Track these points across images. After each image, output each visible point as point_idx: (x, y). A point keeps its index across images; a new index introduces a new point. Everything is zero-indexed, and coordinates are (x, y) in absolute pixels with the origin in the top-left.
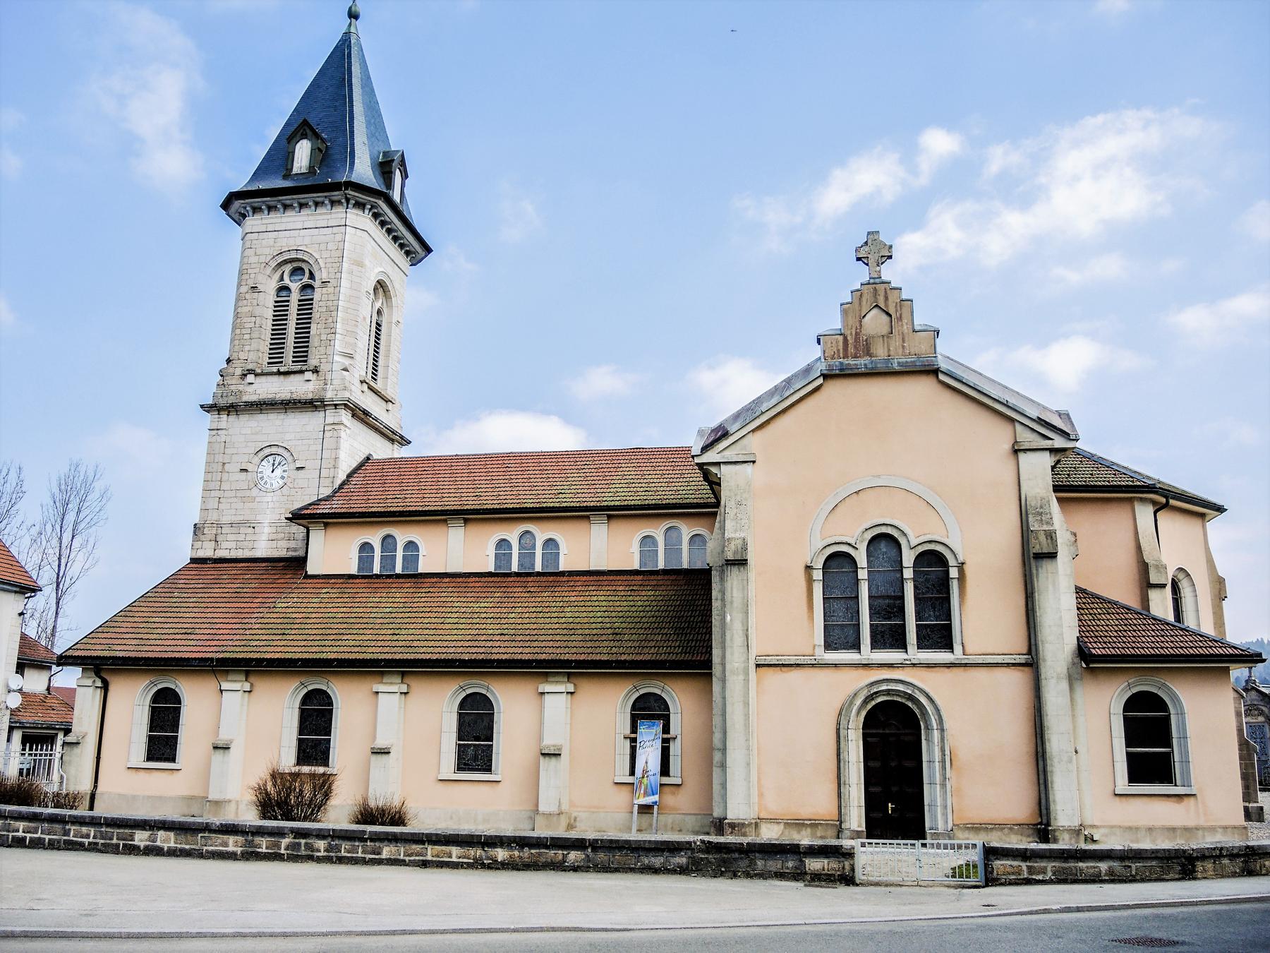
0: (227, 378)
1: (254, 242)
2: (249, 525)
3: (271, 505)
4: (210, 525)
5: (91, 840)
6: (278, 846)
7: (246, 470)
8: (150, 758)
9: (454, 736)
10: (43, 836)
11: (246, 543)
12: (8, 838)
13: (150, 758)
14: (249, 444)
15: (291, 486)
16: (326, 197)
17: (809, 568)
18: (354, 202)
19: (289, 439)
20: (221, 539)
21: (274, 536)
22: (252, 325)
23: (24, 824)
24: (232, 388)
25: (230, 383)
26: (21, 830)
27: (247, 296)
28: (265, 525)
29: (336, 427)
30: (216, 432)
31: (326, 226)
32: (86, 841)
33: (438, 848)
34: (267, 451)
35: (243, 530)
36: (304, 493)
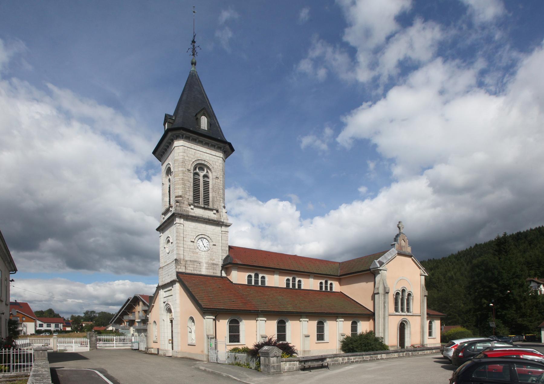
0: (181, 204)
5: (369, 359)
6: (404, 355)
7: (215, 245)
11: (197, 269)
17: (394, 295)
18: (217, 146)
19: (208, 233)
21: (208, 268)
22: (189, 185)
25: (183, 206)
29: (227, 233)
30: (179, 224)
31: (194, 148)
32: (368, 359)
33: (427, 351)
34: (201, 236)
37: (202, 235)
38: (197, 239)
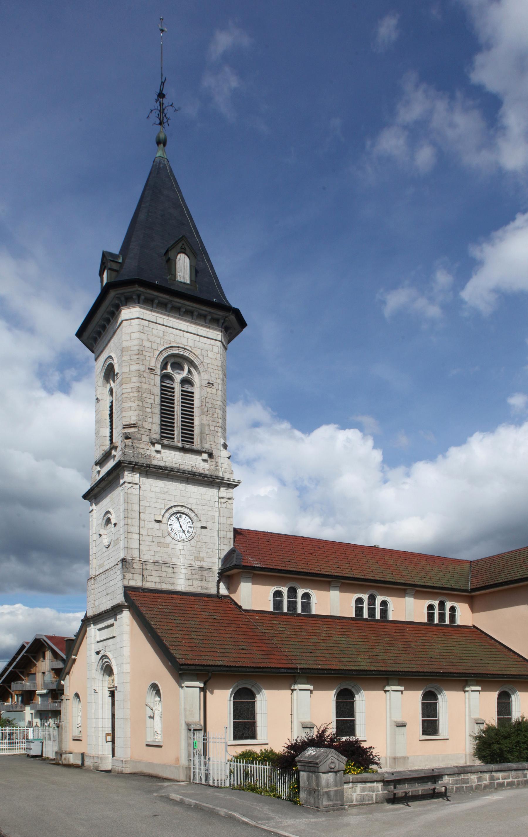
0: (136, 441)
1: (146, 328)
2: (169, 565)
3: (182, 552)
4: (138, 562)
7: (205, 528)
8: (235, 738)
9: (420, 715)
10: (514, 780)
11: (168, 579)
12: (494, 784)
13: (235, 738)
14: (159, 500)
15: (197, 540)
16: (210, 312)
19: (191, 503)
20: (147, 574)
21: (190, 577)
23: (502, 774)
24: (141, 451)
26: (501, 778)
27: (145, 375)
28: (182, 567)
30: (131, 485)
34: (175, 509)
35: (163, 569)
36: (207, 547)
37: (178, 506)
38: (167, 515)
